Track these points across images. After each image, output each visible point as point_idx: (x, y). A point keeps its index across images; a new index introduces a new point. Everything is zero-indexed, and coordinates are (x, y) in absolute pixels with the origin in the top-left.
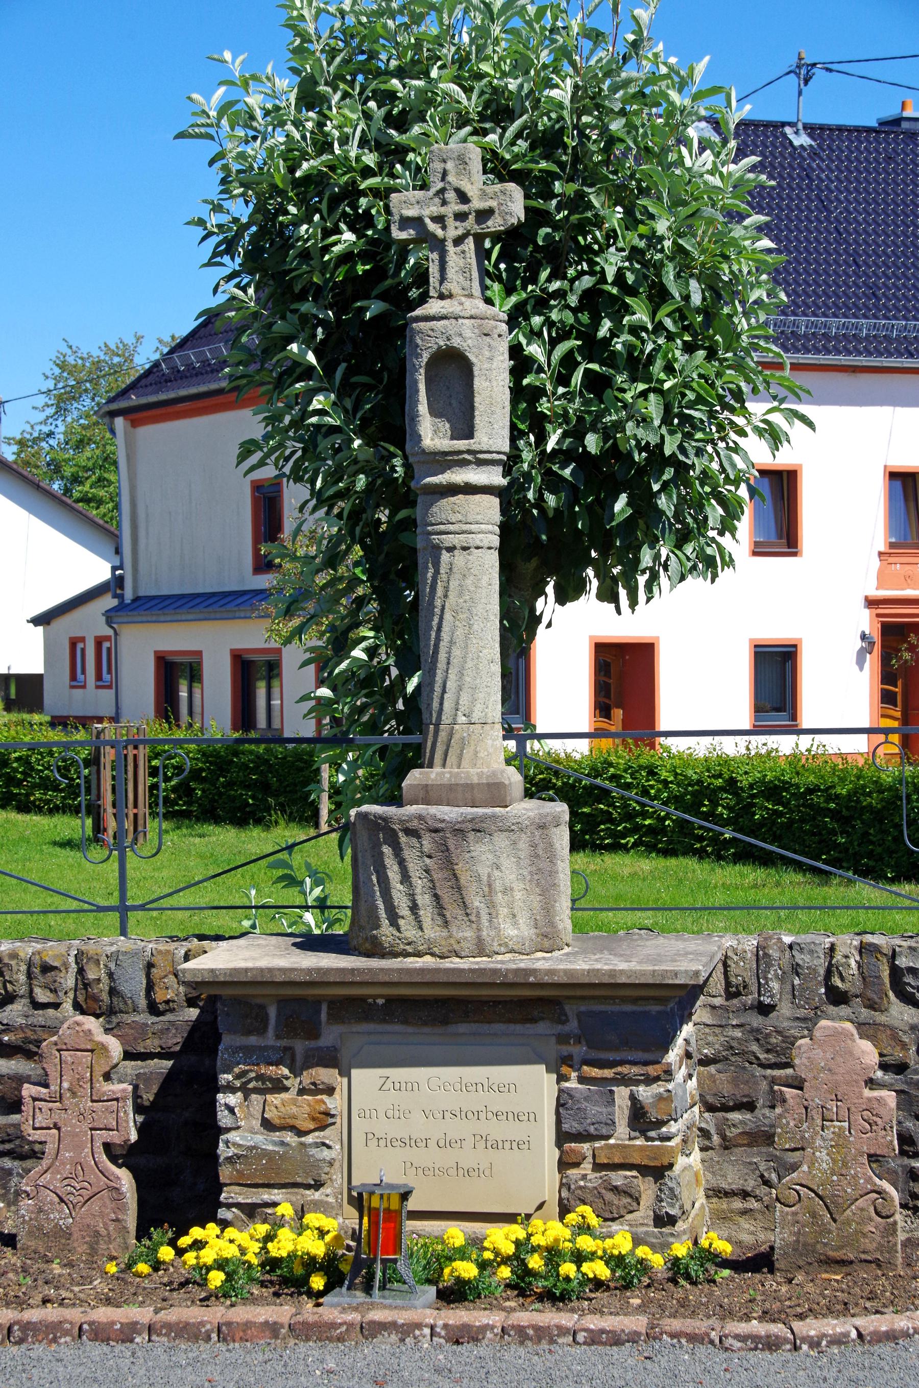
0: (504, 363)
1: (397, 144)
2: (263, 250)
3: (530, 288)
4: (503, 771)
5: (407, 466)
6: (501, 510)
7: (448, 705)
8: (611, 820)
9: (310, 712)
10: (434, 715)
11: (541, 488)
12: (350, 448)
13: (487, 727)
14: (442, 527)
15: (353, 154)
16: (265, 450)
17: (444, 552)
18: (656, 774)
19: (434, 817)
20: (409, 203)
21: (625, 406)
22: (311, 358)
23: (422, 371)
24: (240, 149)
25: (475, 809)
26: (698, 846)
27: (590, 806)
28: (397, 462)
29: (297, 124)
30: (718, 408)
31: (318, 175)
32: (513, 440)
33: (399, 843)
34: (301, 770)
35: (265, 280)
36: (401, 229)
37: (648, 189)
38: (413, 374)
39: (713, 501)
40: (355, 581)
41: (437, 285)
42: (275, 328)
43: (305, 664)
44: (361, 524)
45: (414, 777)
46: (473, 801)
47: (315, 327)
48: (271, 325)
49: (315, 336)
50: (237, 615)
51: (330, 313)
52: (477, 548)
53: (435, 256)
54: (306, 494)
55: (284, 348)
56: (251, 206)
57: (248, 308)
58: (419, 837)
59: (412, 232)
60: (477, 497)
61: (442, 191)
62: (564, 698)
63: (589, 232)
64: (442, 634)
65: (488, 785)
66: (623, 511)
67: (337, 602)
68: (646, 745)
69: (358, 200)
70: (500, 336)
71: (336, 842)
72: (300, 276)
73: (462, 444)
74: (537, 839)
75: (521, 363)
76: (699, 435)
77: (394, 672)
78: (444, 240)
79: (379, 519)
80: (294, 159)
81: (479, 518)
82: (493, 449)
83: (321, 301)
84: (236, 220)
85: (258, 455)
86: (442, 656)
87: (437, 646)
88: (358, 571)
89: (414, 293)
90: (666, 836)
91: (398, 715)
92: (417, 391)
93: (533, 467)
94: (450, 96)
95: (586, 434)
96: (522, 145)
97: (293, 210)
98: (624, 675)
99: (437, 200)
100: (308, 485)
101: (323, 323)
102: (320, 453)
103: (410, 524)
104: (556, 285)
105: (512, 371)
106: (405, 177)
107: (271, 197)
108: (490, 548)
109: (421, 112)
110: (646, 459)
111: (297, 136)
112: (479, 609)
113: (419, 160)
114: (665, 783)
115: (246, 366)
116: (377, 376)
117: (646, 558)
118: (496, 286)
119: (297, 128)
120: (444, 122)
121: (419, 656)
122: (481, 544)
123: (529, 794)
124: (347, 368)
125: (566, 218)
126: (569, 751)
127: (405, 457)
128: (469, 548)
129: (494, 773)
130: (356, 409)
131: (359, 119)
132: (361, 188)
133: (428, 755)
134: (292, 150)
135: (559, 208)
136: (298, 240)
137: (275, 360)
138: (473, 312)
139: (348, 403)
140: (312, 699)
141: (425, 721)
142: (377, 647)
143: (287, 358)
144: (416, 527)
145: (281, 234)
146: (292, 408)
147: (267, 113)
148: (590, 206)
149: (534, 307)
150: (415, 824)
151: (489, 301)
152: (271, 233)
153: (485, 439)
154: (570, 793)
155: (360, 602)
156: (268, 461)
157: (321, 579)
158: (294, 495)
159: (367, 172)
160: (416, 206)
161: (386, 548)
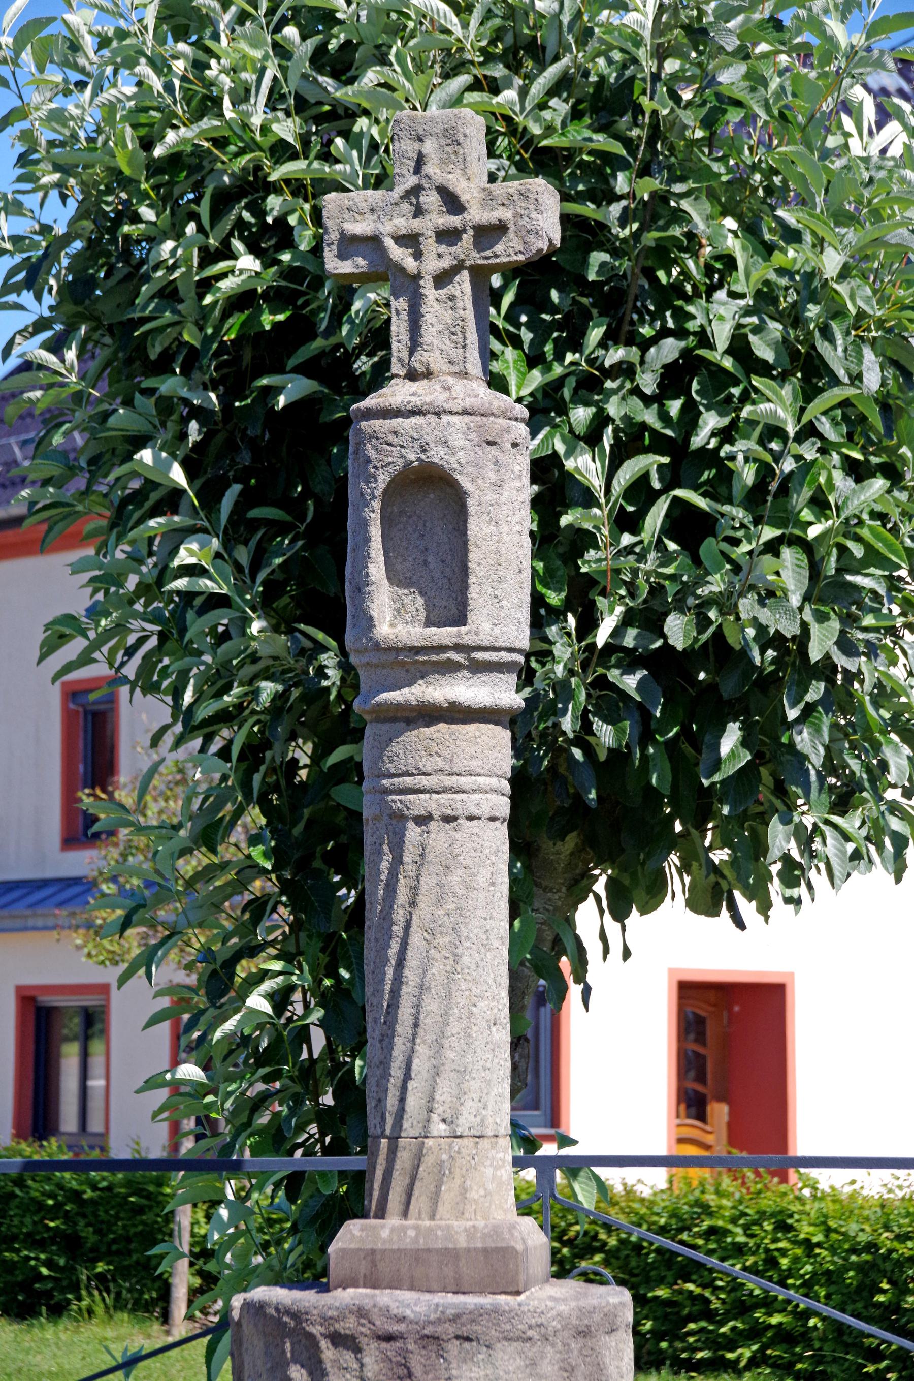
0: (521, 490)
1: (335, 104)
2: (92, 282)
3: (569, 357)
4: (513, 1227)
5: (346, 666)
6: (514, 747)
7: (413, 1102)
8: (709, 1315)
9: (161, 1110)
10: (390, 1121)
11: (586, 712)
12: (244, 634)
13: (485, 1143)
14: (408, 781)
15: (256, 121)
16: (92, 634)
17: (411, 824)
18: (790, 1228)
19: (386, 1312)
20: (354, 212)
21: (737, 569)
22: (178, 475)
23: (377, 505)
24: (53, 106)
25: (461, 1298)
26: (870, 1369)
27: (670, 1286)
28: (328, 659)
29: (160, 65)
30: (903, 573)
31: (193, 154)
32: (537, 624)
33: (320, 1361)
34: (139, 1210)
35: (96, 336)
36: (342, 256)
37: (785, 187)
38: (359, 511)
39: (893, 736)
40: (250, 869)
41: (405, 355)
42: (112, 421)
43: (155, 1020)
44: (263, 768)
45: (352, 1235)
46: (458, 1280)
47: (185, 421)
48: (106, 416)
49: (184, 436)
50: (31, 922)
51: (213, 396)
52: (471, 818)
53: (401, 304)
54: (164, 714)
55: (129, 457)
56: (72, 204)
57: (63, 385)
58: (357, 1350)
59: (361, 261)
60: (472, 728)
61: (416, 190)
62: (622, 1089)
63: (675, 261)
64: (406, 972)
65: (486, 1251)
66: (733, 754)
67: (217, 907)
68: (773, 1174)
69: (264, 199)
70: (515, 445)
71: (204, 1351)
72: (160, 330)
73: (445, 635)
74: (574, 1358)
75: (553, 487)
76: (869, 620)
77: (318, 1039)
78: (418, 277)
79: (295, 761)
80: (151, 125)
81: (474, 764)
82: (500, 643)
83: (196, 375)
84: (45, 229)
85: (77, 645)
86: (405, 1013)
87: (395, 994)
88: (257, 852)
89: (363, 364)
90: (811, 1347)
91: (323, 1117)
92: (367, 540)
93: (571, 672)
94: (432, 21)
95: (666, 614)
96: (560, 106)
97: (147, 213)
98: (731, 1043)
99: (406, 207)
100: (169, 699)
101: (198, 413)
102: (191, 642)
103: (352, 771)
104: (615, 355)
105: (536, 503)
106: (350, 163)
107: (109, 191)
108: (493, 819)
109: (378, 47)
110: (774, 661)
111: (157, 84)
112: (473, 928)
113: (375, 131)
114: (809, 1246)
115: (59, 487)
116: (295, 507)
117: (780, 840)
118: (510, 353)
119: (158, 72)
120: (420, 67)
121: (363, 1009)
122: (477, 812)
123: (562, 1269)
124: (241, 494)
125: (636, 236)
126: (630, 1182)
127: (343, 652)
128: (455, 818)
129: (496, 1230)
130: (256, 564)
131: (266, 57)
132: (273, 178)
133: (376, 1194)
134: (146, 110)
135: (624, 221)
136: (156, 268)
137: (111, 477)
138: (469, 403)
139: (243, 555)
140: (165, 1084)
141: (371, 1131)
142: (290, 988)
143: (134, 474)
144: (361, 778)
145: (126, 255)
146: (141, 562)
147: (104, 42)
148: (679, 216)
149: (576, 391)
150: (349, 1325)
151: (497, 383)
152: (109, 254)
153: (487, 626)
154: (634, 1266)
155: (259, 908)
156: (97, 655)
157: (189, 866)
158: (140, 717)
159: (281, 151)
160: (370, 217)
161: (306, 812)
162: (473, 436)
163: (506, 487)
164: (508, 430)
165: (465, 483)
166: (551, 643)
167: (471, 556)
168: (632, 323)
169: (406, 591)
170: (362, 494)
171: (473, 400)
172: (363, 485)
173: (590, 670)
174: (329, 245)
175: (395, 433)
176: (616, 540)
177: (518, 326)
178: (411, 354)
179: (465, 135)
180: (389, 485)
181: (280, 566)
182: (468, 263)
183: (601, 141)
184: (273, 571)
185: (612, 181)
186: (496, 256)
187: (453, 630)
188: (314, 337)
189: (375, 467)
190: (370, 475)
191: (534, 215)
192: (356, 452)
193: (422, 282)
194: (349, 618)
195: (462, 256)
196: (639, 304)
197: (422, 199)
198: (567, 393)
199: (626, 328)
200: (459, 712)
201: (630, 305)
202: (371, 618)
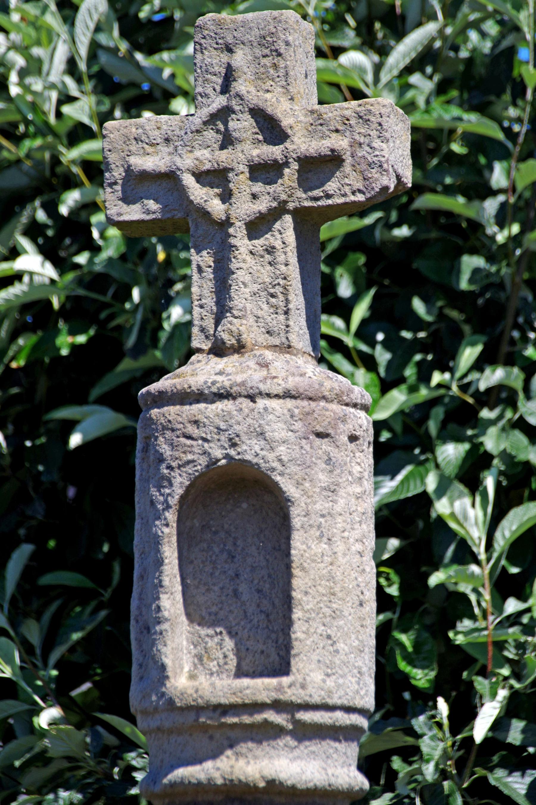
3: (437, 378)
23: (171, 516)
36: (127, 199)
38: (148, 525)
41: (209, 323)
59: (152, 205)
61: (224, 114)
70: (353, 438)
73: (261, 688)
75: (410, 533)
78: (227, 223)
82: (335, 700)
92: (159, 562)
93: (444, 774)
104: (494, 376)
124: (33, 557)
130: (50, 642)
138: (292, 383)
139: (33, 632)
149: (443, 425)
153: (317, 677)
160: (164, 149)
162: (298, 425)
163: (342, 492)
164: (344, 419)
165: (288, 487)
166: (418, 736)
167: (296, 582)
168: (512, 342)
169: (211, 631)
170: (152, 503)
171: (297, 379)
172: (154, 491)
173: (467, 772)
174: (111, 185)
175: (196, 422)
176: (499, 607)
177: (372, 344)
178: (217, 323)
179: (287, 44)
180: (188, 489)
181: (78, 642)
182: (291, 206)
183: (473, 122)
184: (72, 650)
185: (486, 173)
186: (328, 196)
187: (273, 681)
188: (120, 356)
189: (170, 467)
190: (164, 478)
191: (377, 143)
192: (146, 449)
193: (231, 230)
194: (135, 668)
195: (284, 197)
196: (521, 320)
197: (232, 125)
198: (433, 427)
199: (505, 348)
200: (280, 793)
201: (510, 321)
202: (163, 667)
